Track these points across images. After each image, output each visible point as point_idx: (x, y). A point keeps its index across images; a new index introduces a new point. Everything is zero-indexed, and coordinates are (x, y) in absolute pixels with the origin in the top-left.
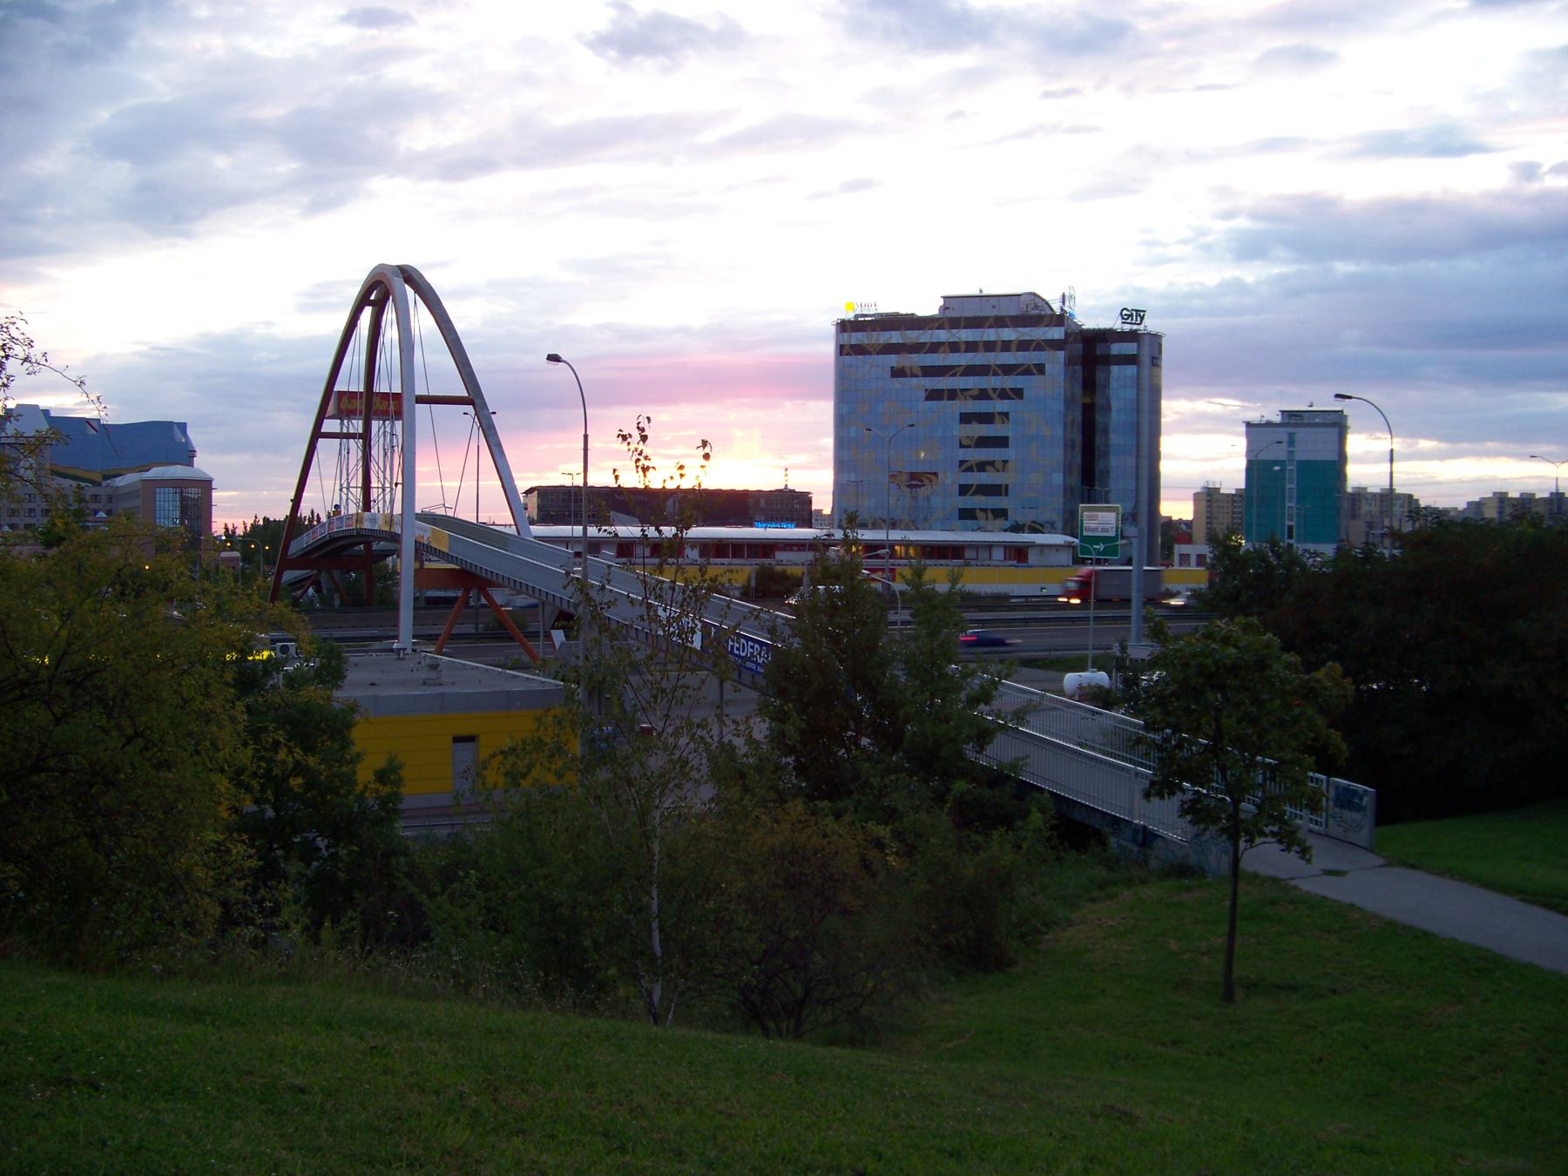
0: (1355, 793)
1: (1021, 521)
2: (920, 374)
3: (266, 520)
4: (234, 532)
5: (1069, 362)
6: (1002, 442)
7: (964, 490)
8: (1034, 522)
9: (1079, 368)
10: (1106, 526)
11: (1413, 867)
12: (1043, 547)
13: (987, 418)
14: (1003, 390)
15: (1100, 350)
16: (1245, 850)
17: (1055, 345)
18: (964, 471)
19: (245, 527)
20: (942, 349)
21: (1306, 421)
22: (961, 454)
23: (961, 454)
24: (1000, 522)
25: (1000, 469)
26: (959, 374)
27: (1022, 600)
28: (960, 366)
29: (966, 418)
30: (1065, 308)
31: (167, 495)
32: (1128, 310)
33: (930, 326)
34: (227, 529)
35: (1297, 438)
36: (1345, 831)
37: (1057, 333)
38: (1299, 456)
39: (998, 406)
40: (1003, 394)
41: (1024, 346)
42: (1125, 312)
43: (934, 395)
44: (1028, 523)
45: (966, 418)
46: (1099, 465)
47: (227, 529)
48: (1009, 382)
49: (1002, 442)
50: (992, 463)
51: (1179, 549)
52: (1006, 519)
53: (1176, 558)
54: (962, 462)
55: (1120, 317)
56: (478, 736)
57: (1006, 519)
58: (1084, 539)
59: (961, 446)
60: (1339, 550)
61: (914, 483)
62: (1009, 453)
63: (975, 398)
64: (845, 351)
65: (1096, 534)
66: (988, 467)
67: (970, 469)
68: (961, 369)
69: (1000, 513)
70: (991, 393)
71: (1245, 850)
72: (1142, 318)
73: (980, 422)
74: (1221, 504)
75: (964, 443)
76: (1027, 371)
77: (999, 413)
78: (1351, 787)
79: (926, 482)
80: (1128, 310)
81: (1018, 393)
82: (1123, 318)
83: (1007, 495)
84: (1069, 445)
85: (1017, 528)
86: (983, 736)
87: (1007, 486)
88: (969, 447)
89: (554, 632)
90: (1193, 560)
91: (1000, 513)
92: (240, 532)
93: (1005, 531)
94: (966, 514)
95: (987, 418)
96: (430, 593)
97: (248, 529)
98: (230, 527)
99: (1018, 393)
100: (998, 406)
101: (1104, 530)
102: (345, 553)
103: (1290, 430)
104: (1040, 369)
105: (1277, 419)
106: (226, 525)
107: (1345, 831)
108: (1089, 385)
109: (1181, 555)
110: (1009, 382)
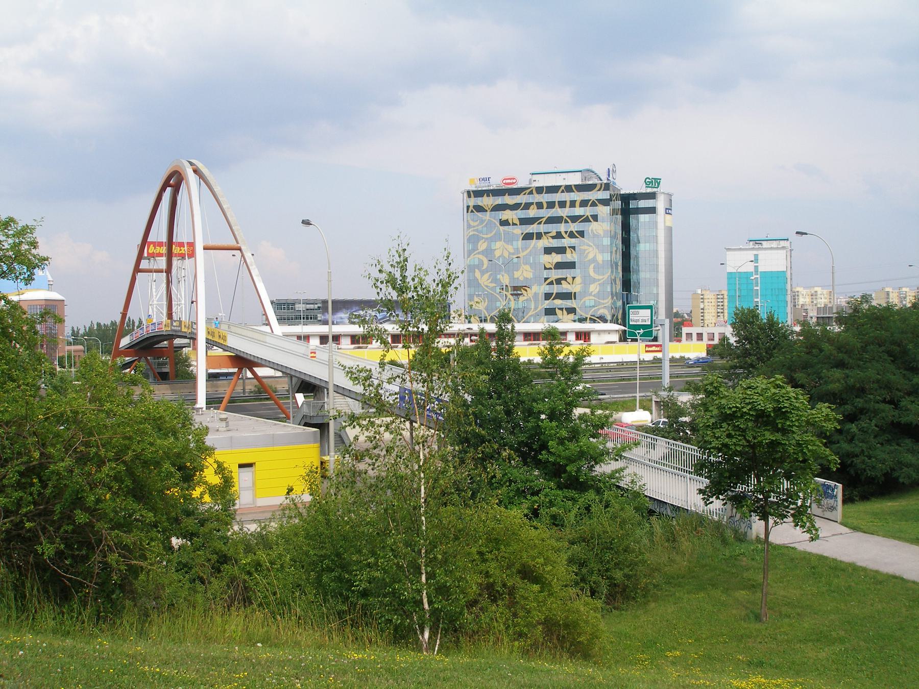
0: (829, 487)
1: (584, 316)
2: (518, 223)
3: (99, 325)
4: (78, 332)
5: (614, 212)
6: (571, 265)
7: (548, 296)
8: (594, 316)
9: (619, 217)
10: (644, 318)
11: (873, 534)
12: (599, 332)
13: (561, 250)
14: (571, 232)
15: (633, 204)
16: (772, 527)
17: (605, 202)
18: (547, 284)
19: (85, 329)
20: (532, 207)
21: (764, 247)
22: (545, 274)
23: (545, 274)
24: (572, 316)
25: (571, 283)
26: (543, 223)
27: (615, 364)
28: (543, 217)
29: (548, 251)
30: (610, 179)
31: (32, 310)
32: (649, 179)
33: (524, 192)
34: (73, 331)
35: (760, 257)
36: (823, 511)
37: (605, 195)
38: (760, 269)
39: (566, 242)
40: (572, 235)
41: (584, 203)
42: (648, 180)
43: (528, 237)
44: (589, 316)
45: (548, 251)
46: (633, 278)
47: (73, 331)
48: (574, 227)
49: (571, 265)
50: (565, 279)
51: (685, 330)
52: (575, 314)
53: (684, 336)
54: (546, 279)
55: (645, 184)
56: (255, 463)
57: (575, 314)
58: (631, 327)
59: (546, 268)
60: (298, 392)
61: (515, 292)
62: (576, 272)
63: (553, 237)
64: (470, 210)
65: (638, 323)
66: (563, 282)
67: (551, 283)
68: (544, 219)
69: (571, 311)
70: (563, 234)
71: (772, 527)
72: (659, 184)
73: (558, 253)
74: (710, 301)
75: (547, 267)
76: (587, 220)
77: (569, 247)
78: (826, 483)
79: (524, 292)
80: (649, 179)
81: (582, 234)
82: (646, 184)
83: (575, 299)
84: (613, 265)
85: (581, 320)
86: (598, 457)
87: (575, 293)
88: (551, 269)
89: (297, 395)
90: (695, 336)
91: (571, 311)
92: (81, 332)
93: (575, 321)
94: (550, 312)
95: (561, 250)
96: (211, 371)
97: (87, 330)
98: (76, 329)
99: (582, 234)
100: (566, 242)
101: (643, 321)
102: (156, 346)
103: (755, 252)
104: (595, 218)
105: (281, 335)
106: (73, 328)
107: (823, 511)
108: (626, 228)
109: (687, 334)
110: (574, 227)
